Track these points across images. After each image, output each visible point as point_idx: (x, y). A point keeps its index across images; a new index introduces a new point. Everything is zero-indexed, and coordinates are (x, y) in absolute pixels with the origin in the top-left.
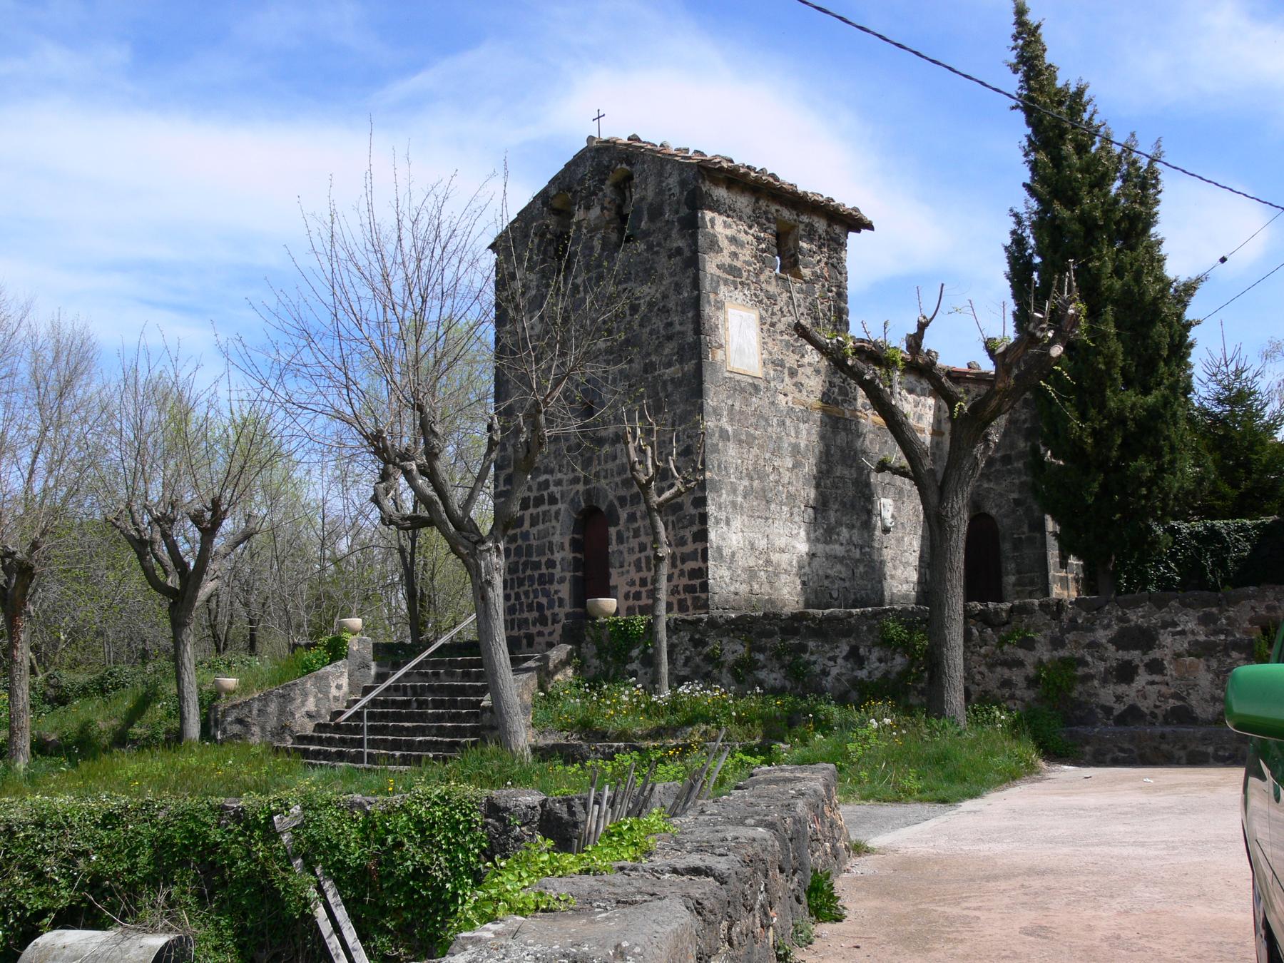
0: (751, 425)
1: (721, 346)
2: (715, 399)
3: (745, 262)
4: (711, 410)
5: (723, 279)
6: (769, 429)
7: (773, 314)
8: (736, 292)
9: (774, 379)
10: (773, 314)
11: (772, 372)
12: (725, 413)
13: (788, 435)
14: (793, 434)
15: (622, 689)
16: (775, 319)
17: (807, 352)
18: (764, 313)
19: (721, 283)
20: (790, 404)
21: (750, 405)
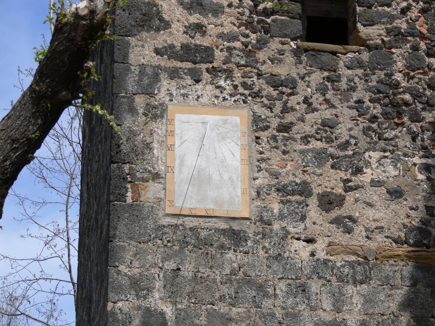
0: (222, 298)
1: (156, 176)
2: (136, 264)
3: (221, 36)
4: (125, 281)
5: (166, 70)
6: (267, 303)
7: (286, 110)
8: (199, 86)
9: (282, 217)
10: (286, 110)
11: (276, 207)
12: (158, 284)
13: (313, 309)
14: (327, 304)
15: (194, 238)
16: (289, 118)
17: (368, 164)
18: (263, 112)
19: (163, 76)
20: (321, 255)
21: (221, 266)
